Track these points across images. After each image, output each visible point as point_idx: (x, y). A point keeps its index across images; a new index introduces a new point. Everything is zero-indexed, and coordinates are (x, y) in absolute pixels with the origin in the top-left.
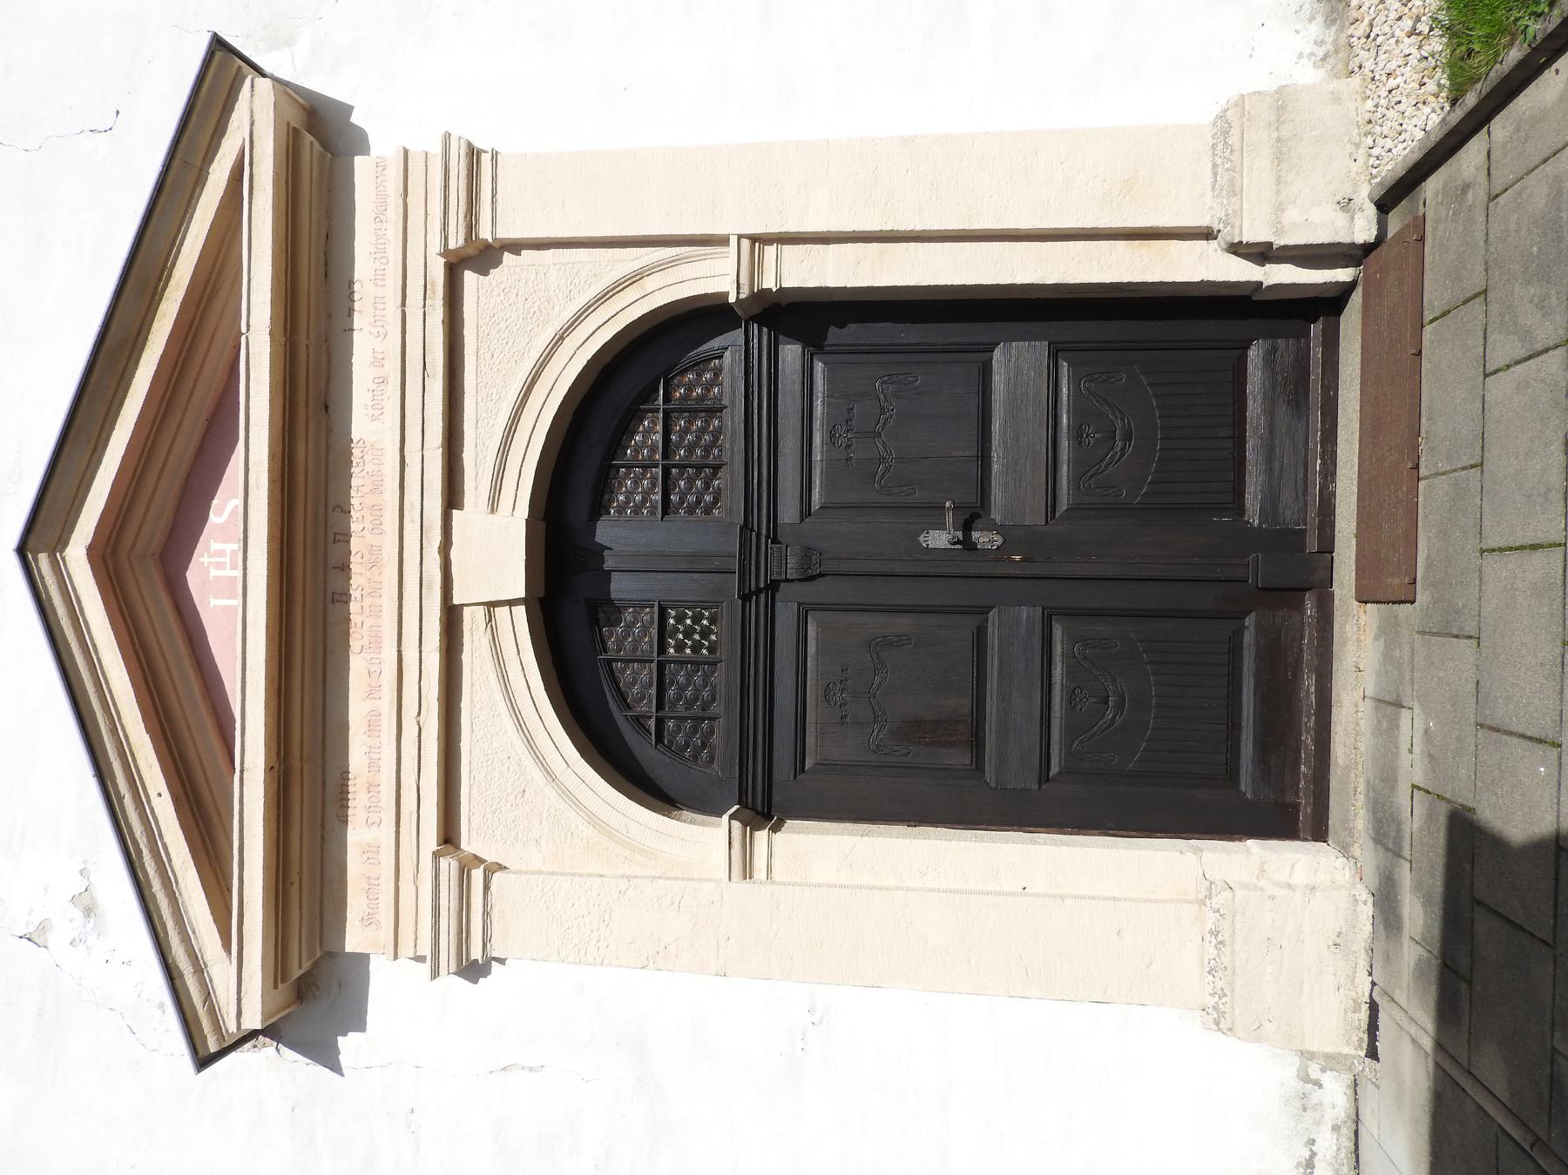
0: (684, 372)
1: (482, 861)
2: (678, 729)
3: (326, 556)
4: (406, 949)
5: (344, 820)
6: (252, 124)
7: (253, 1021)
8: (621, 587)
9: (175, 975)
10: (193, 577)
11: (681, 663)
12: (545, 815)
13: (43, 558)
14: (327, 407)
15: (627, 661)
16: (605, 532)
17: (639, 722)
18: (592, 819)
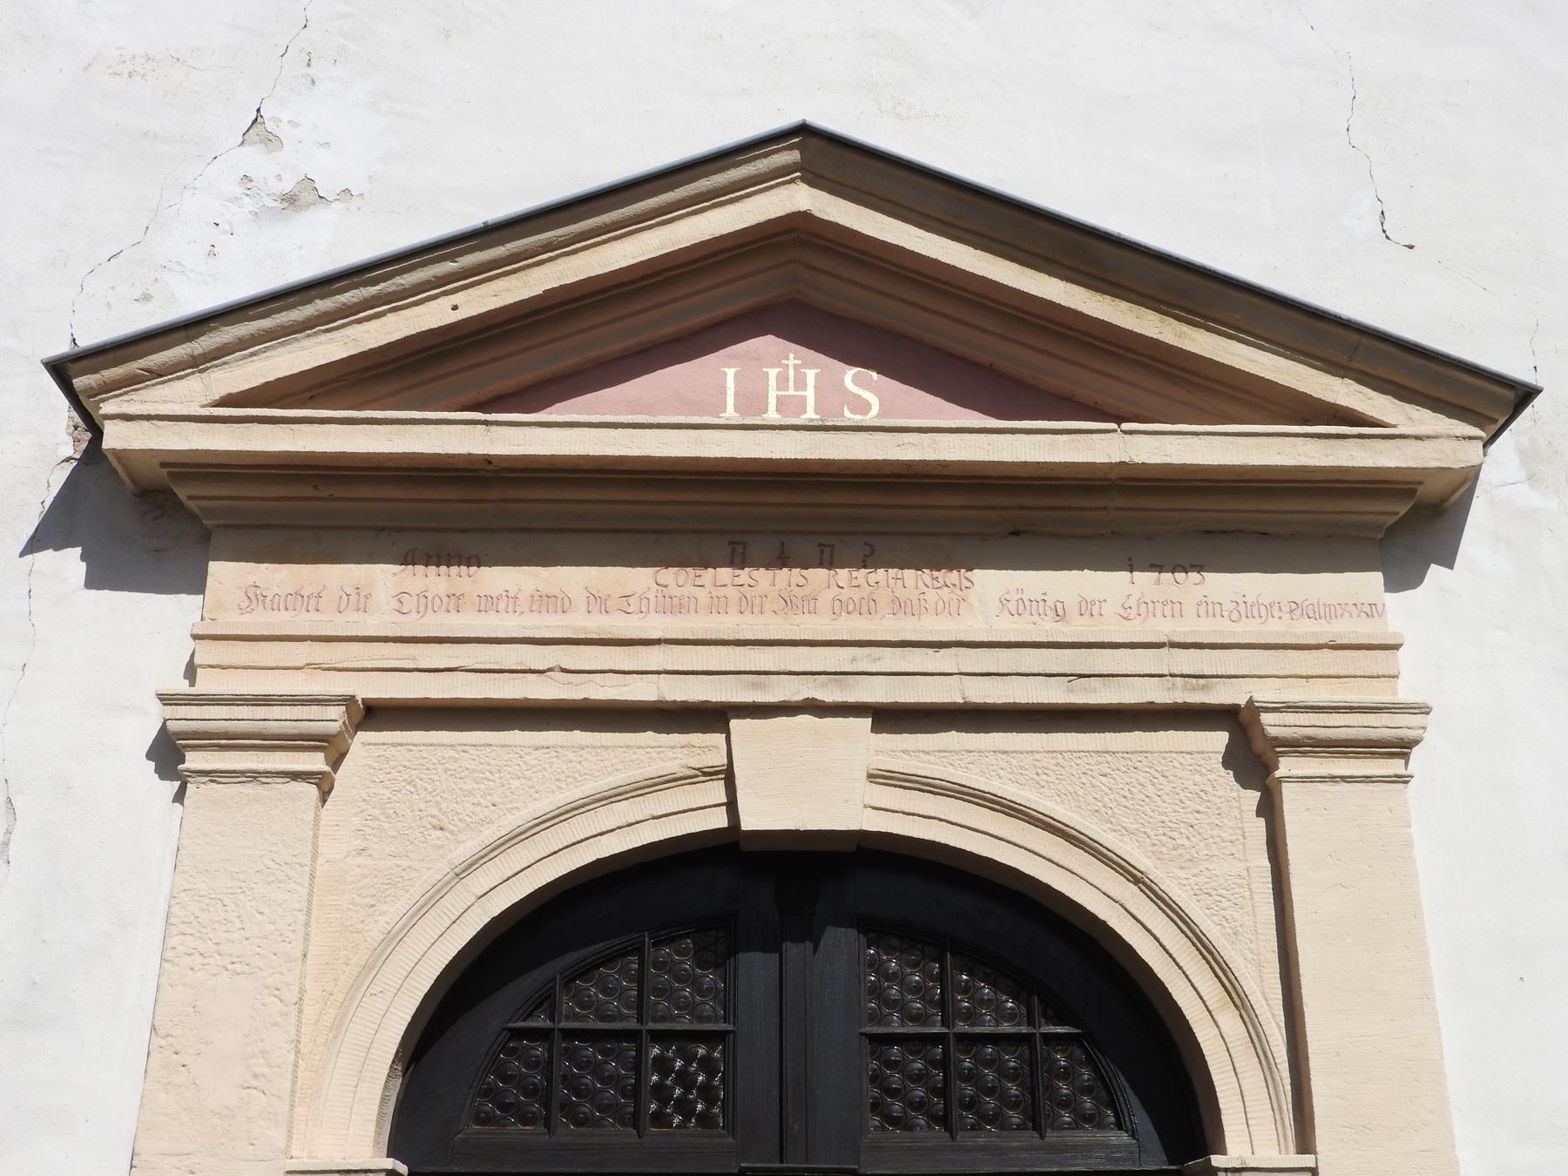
0: (1091, 1062)
1: (336, 764)
2: (533, 1064)
3: (798, 533)
4: (207, 653)
5: (407, 559)
6: (1417, 438)
7: (116, 437)
8: (756, 967)
9: (191, 332)
10: (766, 344)
11: (637, 1066)
12: (405, 863)
13: (794, 156)
14: (1016, 533)
15: (640, 979)
16: (840, 941)
17: (545, 1000)
18: (395, 938)
